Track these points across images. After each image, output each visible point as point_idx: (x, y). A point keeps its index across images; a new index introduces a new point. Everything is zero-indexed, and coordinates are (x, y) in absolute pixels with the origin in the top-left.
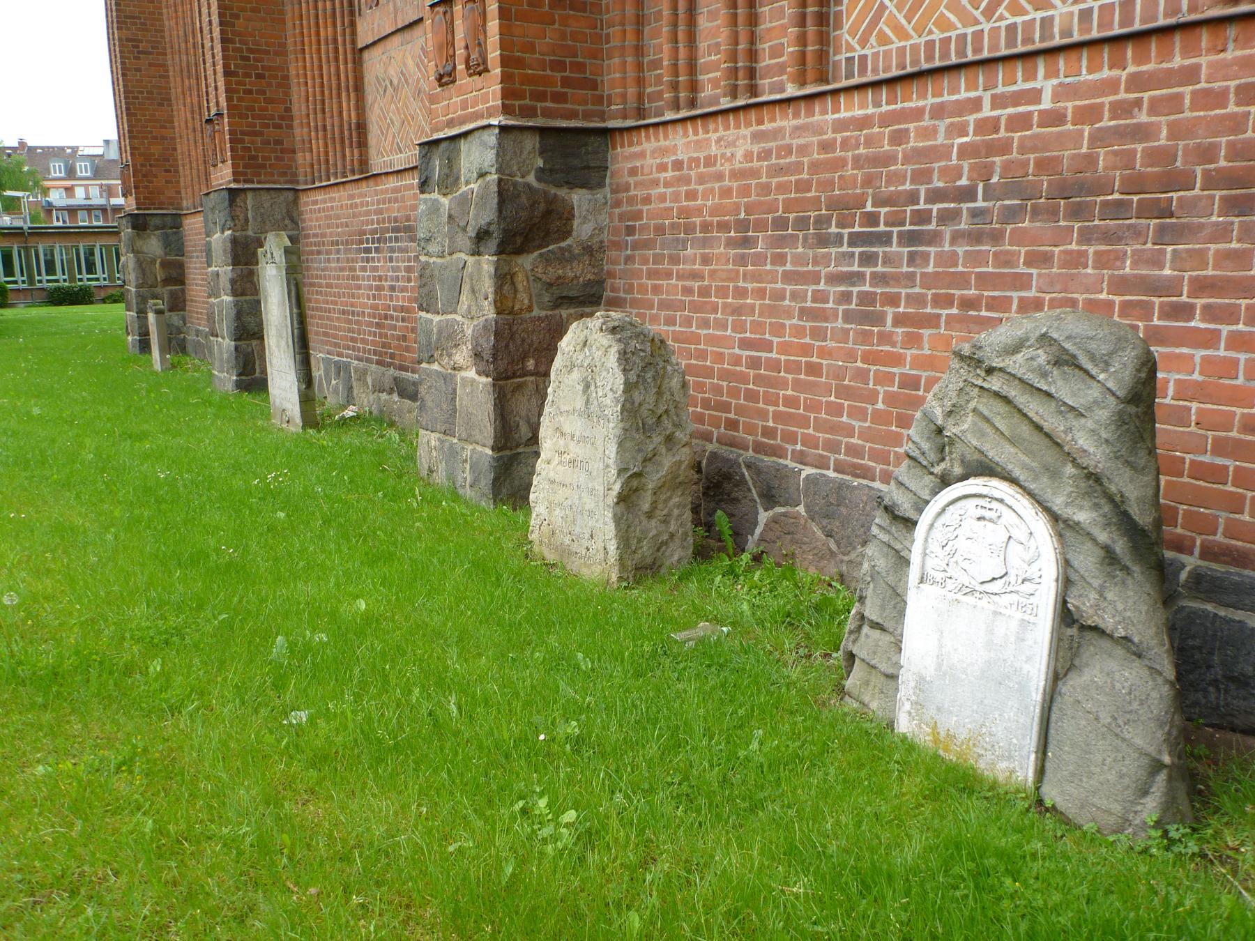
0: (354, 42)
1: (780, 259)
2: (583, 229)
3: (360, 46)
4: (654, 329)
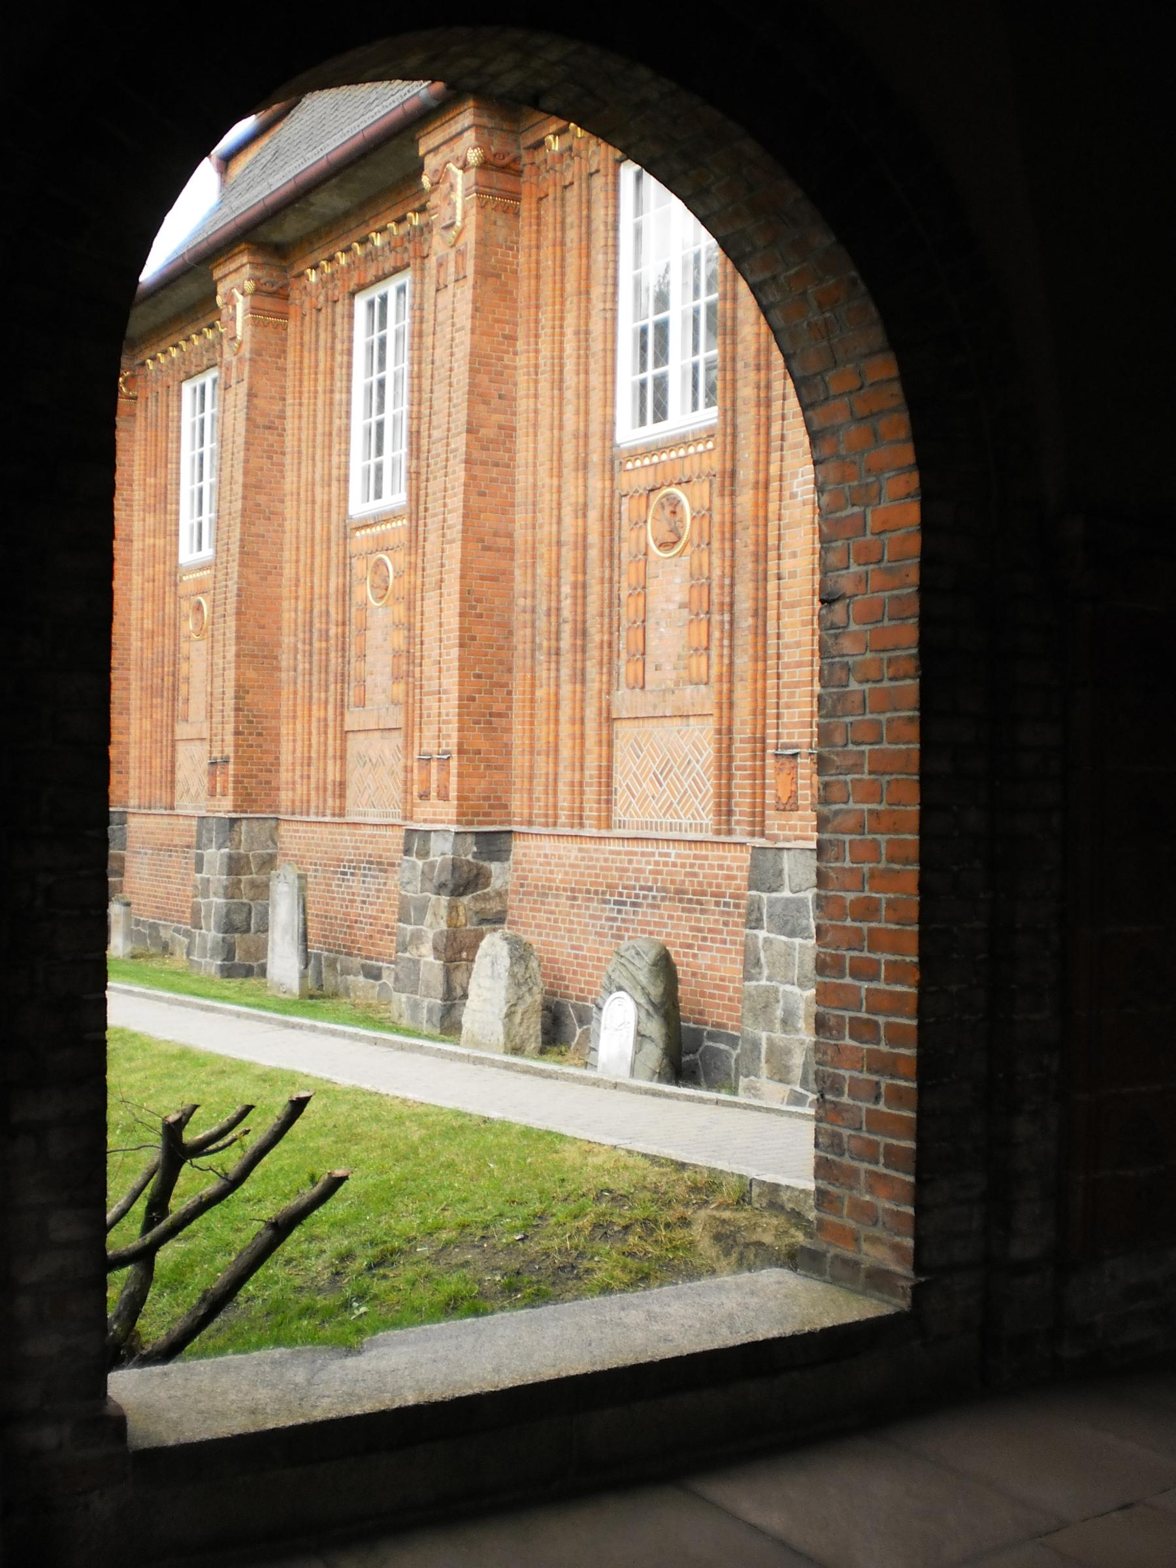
0: (342, 726)
1: (587, 908)
2: (496, 883)
3: (346, 729)
4: (526, 938)
